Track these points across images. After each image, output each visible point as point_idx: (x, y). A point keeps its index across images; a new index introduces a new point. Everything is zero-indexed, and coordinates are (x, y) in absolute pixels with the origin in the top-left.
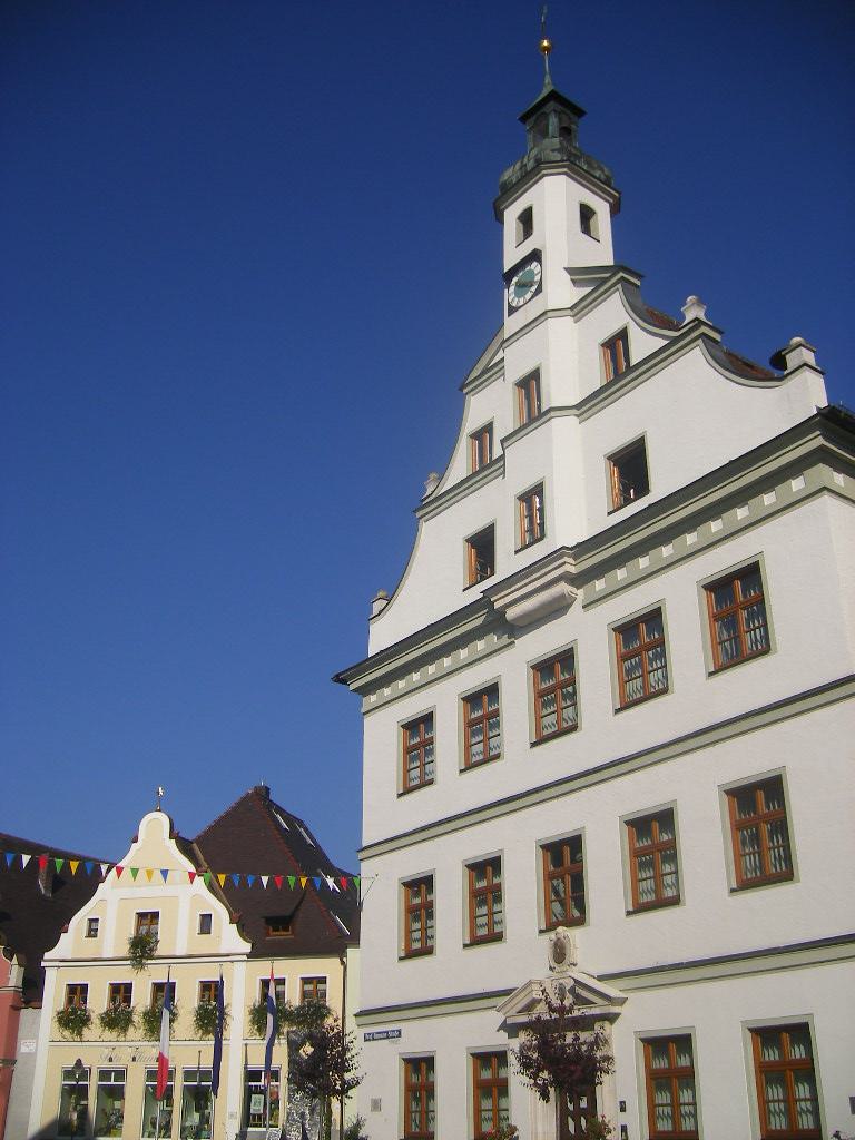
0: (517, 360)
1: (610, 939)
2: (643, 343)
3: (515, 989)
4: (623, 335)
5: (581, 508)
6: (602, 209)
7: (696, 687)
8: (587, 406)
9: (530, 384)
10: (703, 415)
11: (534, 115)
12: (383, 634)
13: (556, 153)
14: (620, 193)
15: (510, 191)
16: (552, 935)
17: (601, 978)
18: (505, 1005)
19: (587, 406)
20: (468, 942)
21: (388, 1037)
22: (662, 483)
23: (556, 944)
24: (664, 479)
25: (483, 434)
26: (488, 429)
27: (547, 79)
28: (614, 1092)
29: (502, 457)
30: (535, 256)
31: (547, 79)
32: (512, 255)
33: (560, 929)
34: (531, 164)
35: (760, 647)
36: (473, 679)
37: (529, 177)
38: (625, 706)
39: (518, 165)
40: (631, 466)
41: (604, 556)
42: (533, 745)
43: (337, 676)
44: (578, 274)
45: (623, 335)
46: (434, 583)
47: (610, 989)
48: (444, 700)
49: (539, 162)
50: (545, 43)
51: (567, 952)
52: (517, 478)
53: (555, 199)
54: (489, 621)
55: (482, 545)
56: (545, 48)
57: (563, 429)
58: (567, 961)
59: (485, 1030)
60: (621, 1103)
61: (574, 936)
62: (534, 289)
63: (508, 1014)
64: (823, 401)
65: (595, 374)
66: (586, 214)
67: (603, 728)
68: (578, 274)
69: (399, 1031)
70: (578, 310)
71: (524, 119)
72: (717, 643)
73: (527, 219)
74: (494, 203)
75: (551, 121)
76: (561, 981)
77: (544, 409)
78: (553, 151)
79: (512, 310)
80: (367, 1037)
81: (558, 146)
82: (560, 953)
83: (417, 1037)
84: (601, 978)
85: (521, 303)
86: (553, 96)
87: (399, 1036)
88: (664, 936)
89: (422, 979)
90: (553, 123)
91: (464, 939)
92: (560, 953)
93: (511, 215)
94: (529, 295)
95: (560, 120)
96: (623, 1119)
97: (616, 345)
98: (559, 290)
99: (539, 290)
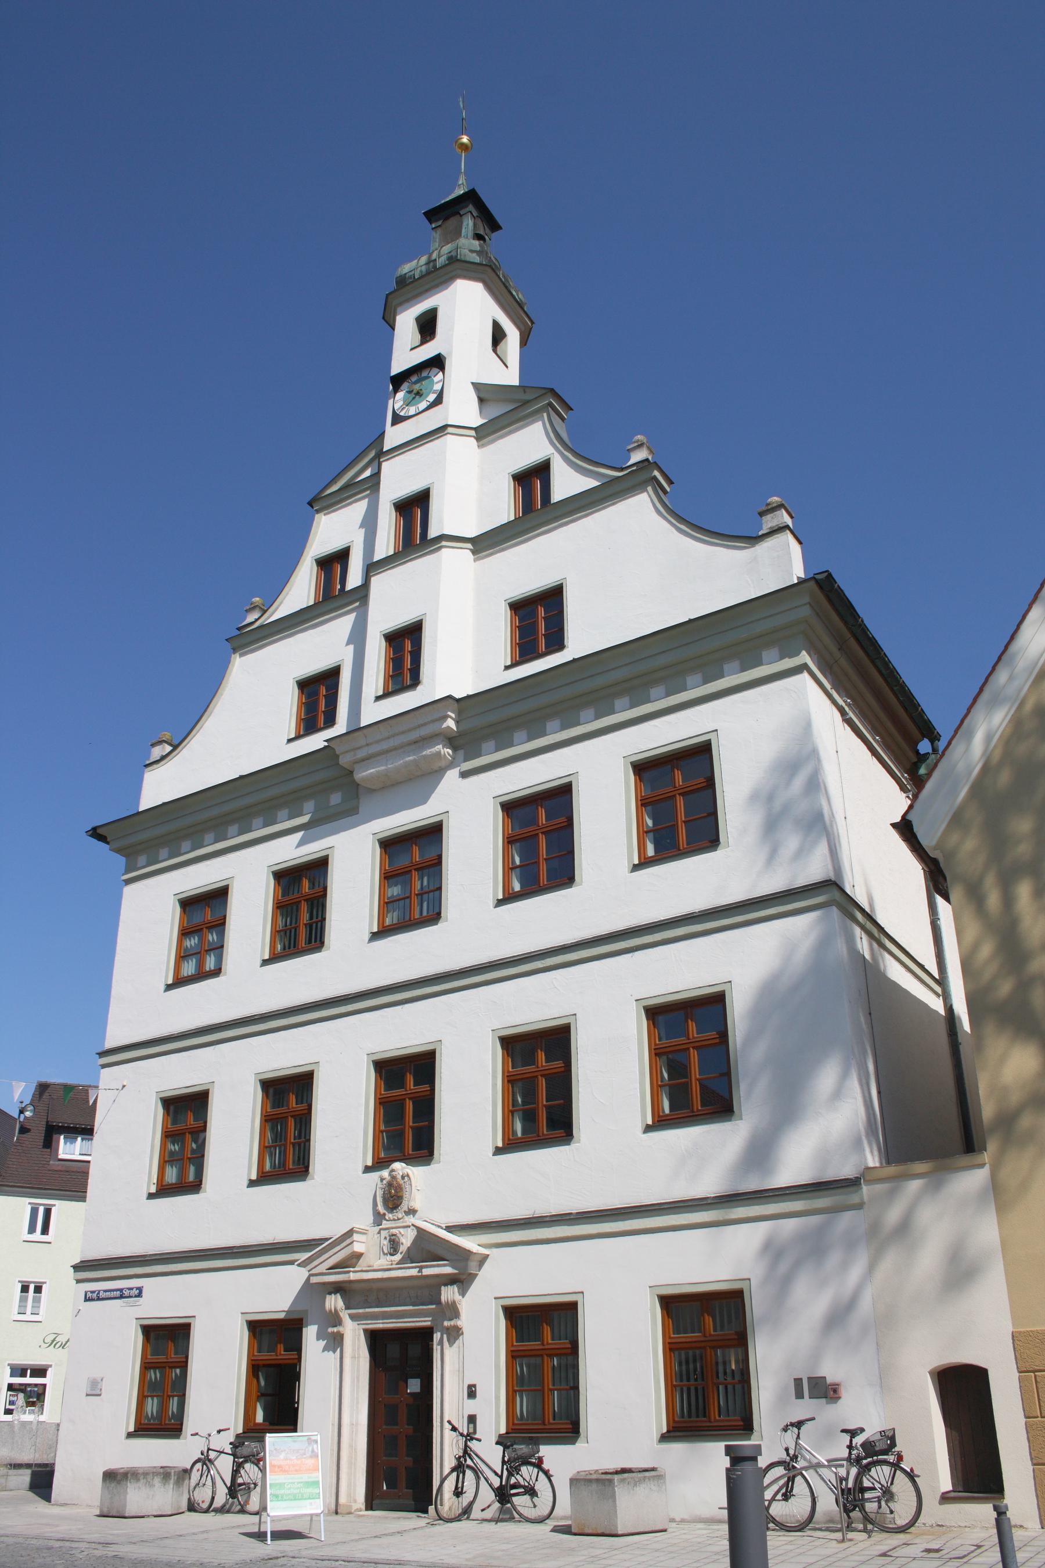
0: (398, 479)
1: (468, 1173)
2: (567, 482)
3: (327, 1239)
4: (541, 471)
5: (468, 657)
6: (513, 335)
7: (250, 975)
8: (485, 544)
9: (414, 507)
10: (635, 571)
11: (443, 214)
12: (162, 785)
13: (474, 255)
14: (532, 323)
15: (408, 288)
16: (385, 1173)
17: (449, 1229)
18: (310, 1260)
19: (485, 544)
20: (369, 1163)
21: (121, 1297)
22: (583, 638)
23: (390, 1185)
24: (583, 638)
25: (334, 563)
26: (342, 556)
27: (462, 180)
28: (461, 1372)
29: (364, 588)
30: (438, 362)
31: (462, 180)
32: (406, 351)
33: (397, 1166)
34: (442, 261)
35: (425, 913)
36: (288, 850)
37: (437, 277)
38: (179, 982)
39: (424, 259)
40: (538, 618)
41: (487, 724)
42: (169, 987)
43: (94, 829)
44: (485, 394)
45: (541, 471)
46: (248, 723)
47: (469, 1243)
48: (248, 876)
49: (453, 260)
50: (465, 139)
51: (406, 1195)
52: (387, 610)
53: (467, 309)
54: (317, 786)
55: (318, 694)
56: (465, 147)
57: (454, 560)
58: (404, 1207)
59: (275, 1291)
60: (470, 1387)
61: (417, 1175)
62: (432, 397)
63: (313, 1272)
64: (798, 571)
65: (503, 509)
66: (498, 336)
67: (353, 948)
68: (485, 394)
69: (140, 1290)
70: (483, 434)
71: (432, 215)
72: (277, 933)
73: (427, 326)
74: (387, 296)
75: (465, 224)
76: (394, 1231)
77: (433, 533)
78: (472, 251)
79: (397, 419)
80: (89, 1295)
81: (478, 249)
82: (393, 1197)
83: (164, 1299)
84: (449, 1229)
85: (412, 411)
86: (471, 197)
87: (140, 1295)
88: (547, 1177)
89: (182, 1223)
90: (468, 224)
91: (249, 1173)
92: (393, 1197)
93: (406, 322)
94: (423, 405)
95: (475, 225)
96: (471, 1407)
97: (532, 480)
98: (463, 408)
99: (439, 401)
